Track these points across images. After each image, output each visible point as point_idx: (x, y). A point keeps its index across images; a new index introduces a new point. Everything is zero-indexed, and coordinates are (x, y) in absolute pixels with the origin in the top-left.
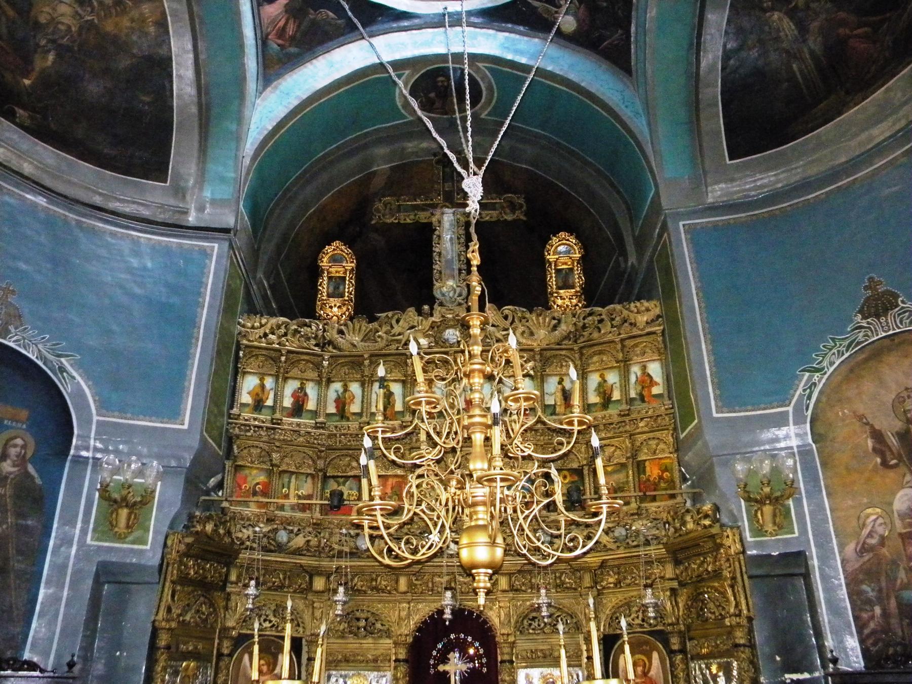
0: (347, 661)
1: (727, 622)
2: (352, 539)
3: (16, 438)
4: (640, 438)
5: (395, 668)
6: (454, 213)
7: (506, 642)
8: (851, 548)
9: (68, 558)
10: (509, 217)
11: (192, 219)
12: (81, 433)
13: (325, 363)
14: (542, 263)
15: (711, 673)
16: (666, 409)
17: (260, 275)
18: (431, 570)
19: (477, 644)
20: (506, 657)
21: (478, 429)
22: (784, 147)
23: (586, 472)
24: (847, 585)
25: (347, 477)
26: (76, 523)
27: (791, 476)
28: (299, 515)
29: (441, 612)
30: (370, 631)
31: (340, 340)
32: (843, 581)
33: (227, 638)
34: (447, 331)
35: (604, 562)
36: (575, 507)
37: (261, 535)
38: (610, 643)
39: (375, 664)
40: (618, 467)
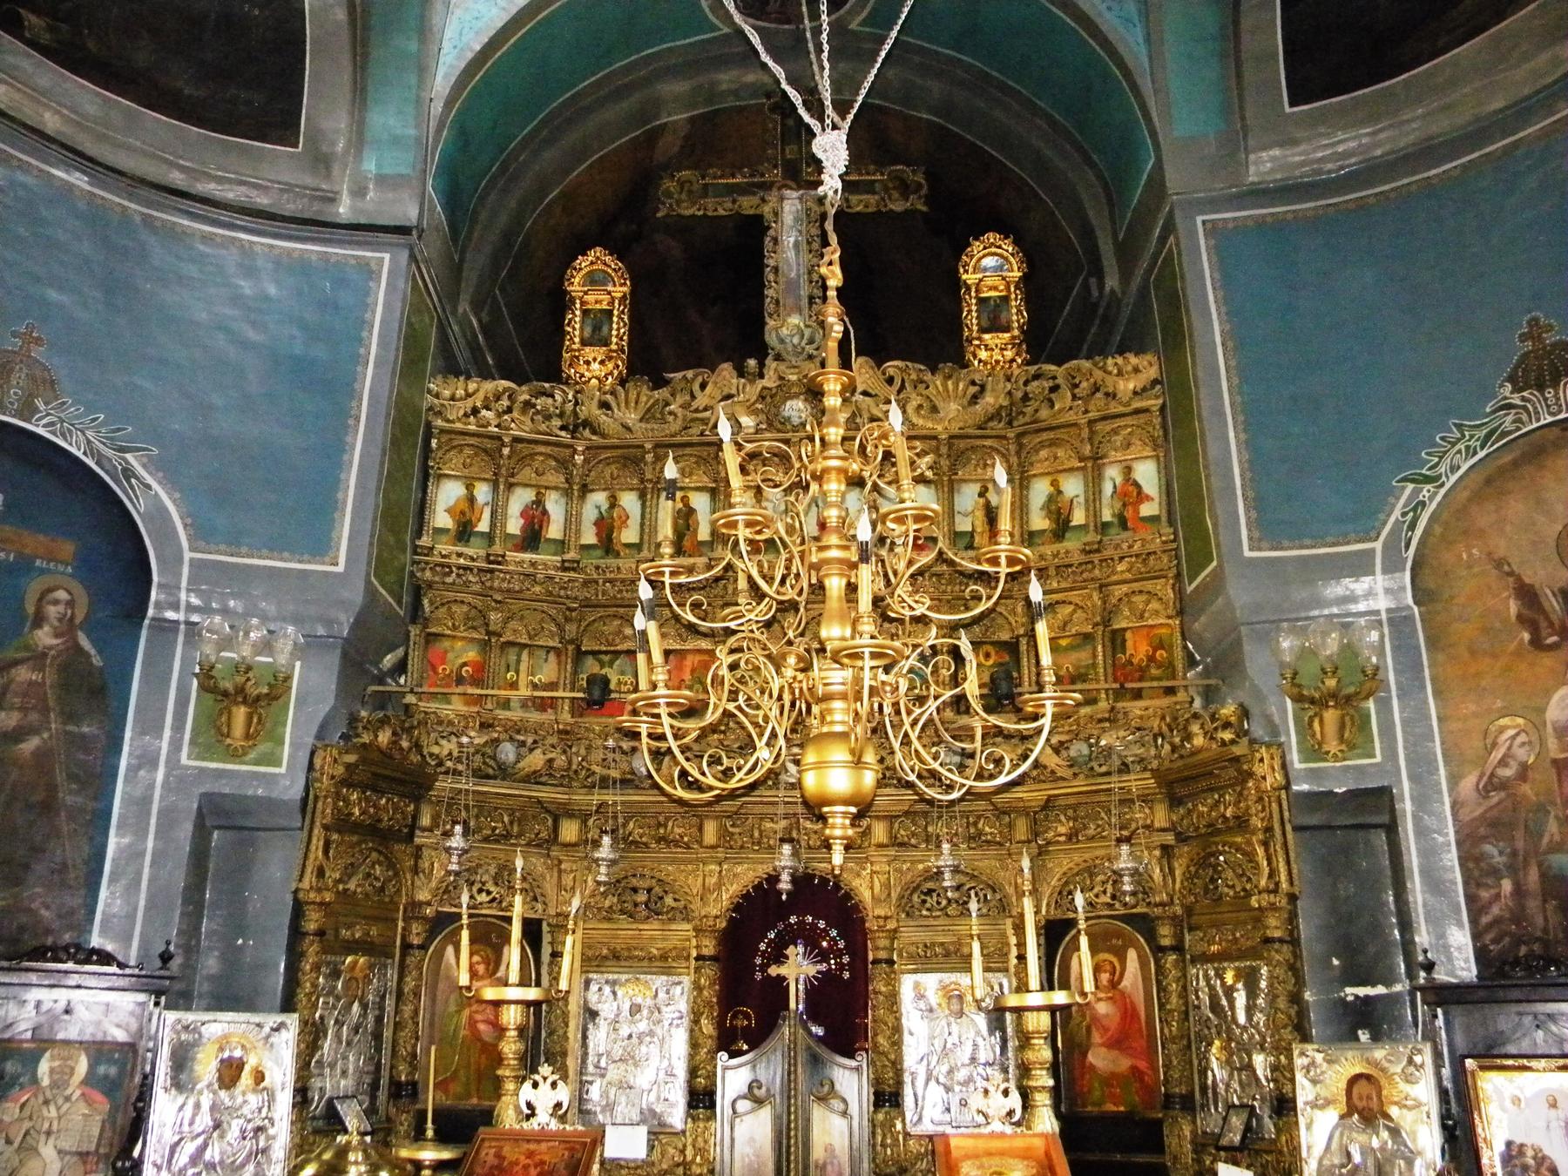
0: (617, 957)
1: (1254, 902)
2: (624, 758)
3: (51, 590)
4: (1119, 591)
5: (697, 970)
6: (800, 198)
7: (881, 929)
8: (1469, 783)
9: (152, 786)
10: (898, 206)
11: (344, 210)
12: (164, 581)
13: (579, 459)
14: (955, 286)
15: (1223, 984)
16: (1164, 542)
17: (464, 306)
18: (758, 809)
19: (834, 933)
20: (882, 955)
21: (835, 569)
22: (1387, 83)
23: (1023, 647)
24: (1459, 844)
25: (617, 654)
26: (162, 728)
27: (1374, 660)
28: (535, 716)
29: (773, 879)
30: (654, 908)
31: (602, 418)
32: (1452, 837)
33: (417, 918)
34: (789, 403)
35: (1049, 799)
36: (1003, 706)
37: (472, 750)
38: (1056, 933)
39: (663, 963)
40: (1078, 640)
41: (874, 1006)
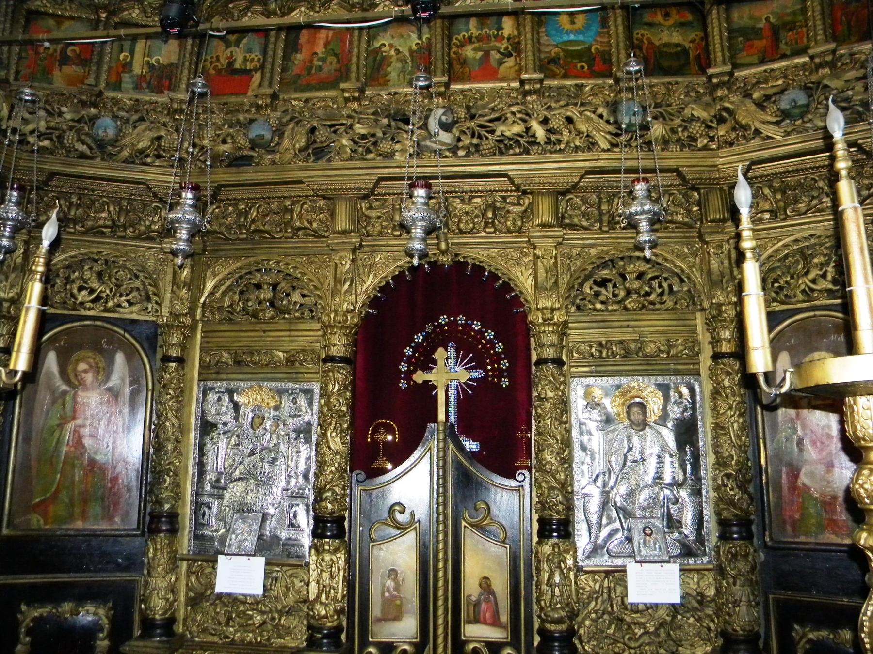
20: (549, 353)
41: (538, 416)
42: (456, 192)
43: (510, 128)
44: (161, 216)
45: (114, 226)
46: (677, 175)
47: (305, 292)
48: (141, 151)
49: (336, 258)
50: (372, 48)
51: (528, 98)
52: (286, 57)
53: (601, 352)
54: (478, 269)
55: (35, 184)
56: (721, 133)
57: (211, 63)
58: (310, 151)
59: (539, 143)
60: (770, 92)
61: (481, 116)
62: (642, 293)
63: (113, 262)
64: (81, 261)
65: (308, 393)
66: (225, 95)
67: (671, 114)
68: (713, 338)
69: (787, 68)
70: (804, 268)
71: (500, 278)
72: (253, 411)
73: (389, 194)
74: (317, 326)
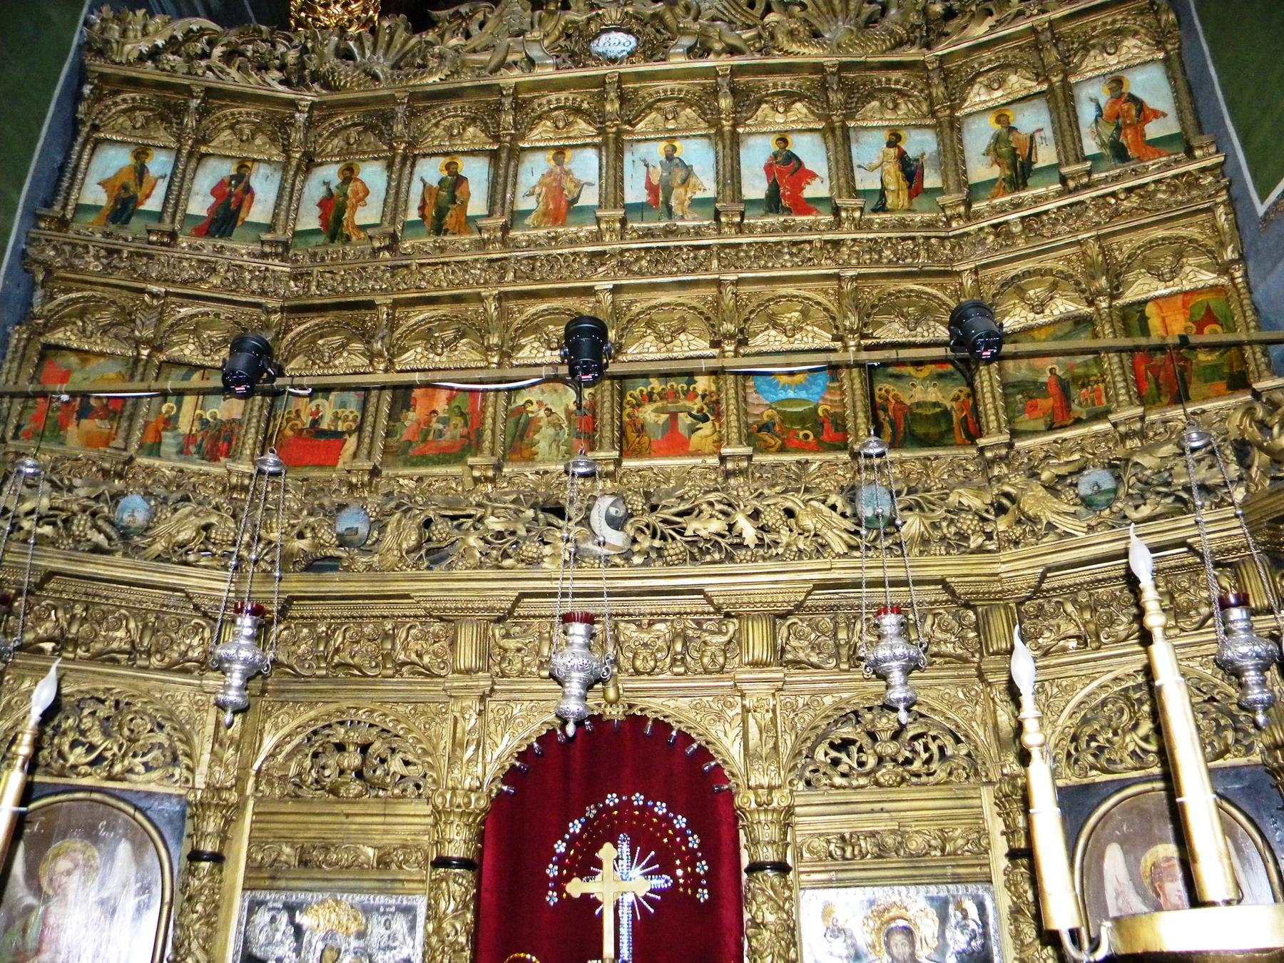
20: (768, 854)
41: (753, 951)
42: (630, 615)
43: (707, 525)
44: (202, 639)
45: (133, 651)
46: (944, 588)
47: (410, 757)
48: (182, 545)
49: (456, 708)
50: (514, 406)
51: (732, 481)
52: (392, 417)
53: (843, 850)
54: (662, 727)
55: (25, 587)
56: (1002, 527)
57: (288, 420)
58: (423, 552)
59: (747, 546)
60: (1063, 471)
61: (667, 507)
62: (901, 759)
63: (127, 704)
64: (79, 701)
65: (408, 911)
66: (306, 466)
67: (931, 503)
68: (1007, 826)
69: (1084, 437)
70: (1131, 718)
71: (693, 741)
72: (324, 939)
73: (534, 617)
74: (428, 809)
